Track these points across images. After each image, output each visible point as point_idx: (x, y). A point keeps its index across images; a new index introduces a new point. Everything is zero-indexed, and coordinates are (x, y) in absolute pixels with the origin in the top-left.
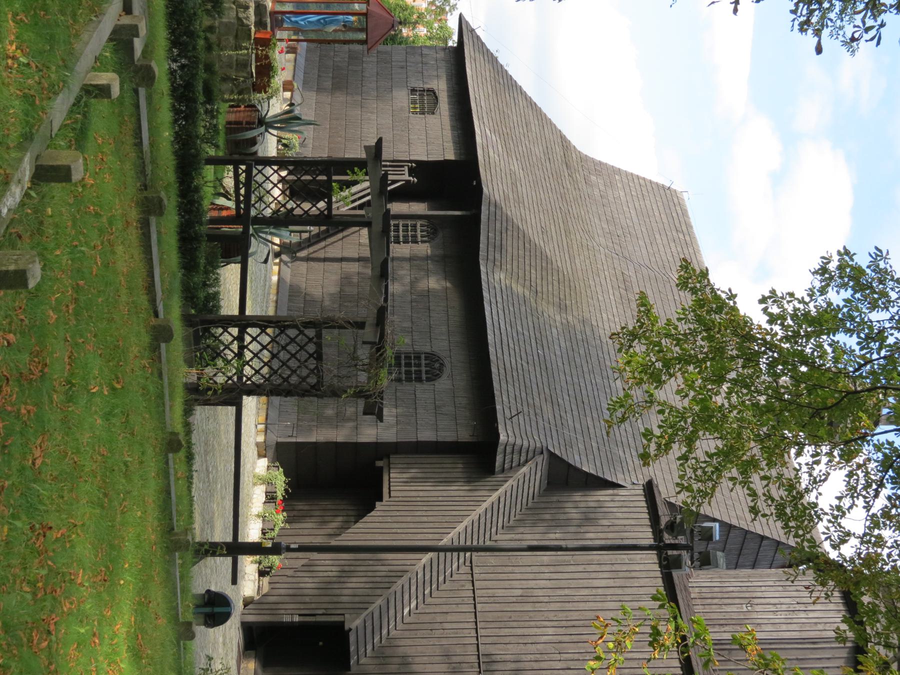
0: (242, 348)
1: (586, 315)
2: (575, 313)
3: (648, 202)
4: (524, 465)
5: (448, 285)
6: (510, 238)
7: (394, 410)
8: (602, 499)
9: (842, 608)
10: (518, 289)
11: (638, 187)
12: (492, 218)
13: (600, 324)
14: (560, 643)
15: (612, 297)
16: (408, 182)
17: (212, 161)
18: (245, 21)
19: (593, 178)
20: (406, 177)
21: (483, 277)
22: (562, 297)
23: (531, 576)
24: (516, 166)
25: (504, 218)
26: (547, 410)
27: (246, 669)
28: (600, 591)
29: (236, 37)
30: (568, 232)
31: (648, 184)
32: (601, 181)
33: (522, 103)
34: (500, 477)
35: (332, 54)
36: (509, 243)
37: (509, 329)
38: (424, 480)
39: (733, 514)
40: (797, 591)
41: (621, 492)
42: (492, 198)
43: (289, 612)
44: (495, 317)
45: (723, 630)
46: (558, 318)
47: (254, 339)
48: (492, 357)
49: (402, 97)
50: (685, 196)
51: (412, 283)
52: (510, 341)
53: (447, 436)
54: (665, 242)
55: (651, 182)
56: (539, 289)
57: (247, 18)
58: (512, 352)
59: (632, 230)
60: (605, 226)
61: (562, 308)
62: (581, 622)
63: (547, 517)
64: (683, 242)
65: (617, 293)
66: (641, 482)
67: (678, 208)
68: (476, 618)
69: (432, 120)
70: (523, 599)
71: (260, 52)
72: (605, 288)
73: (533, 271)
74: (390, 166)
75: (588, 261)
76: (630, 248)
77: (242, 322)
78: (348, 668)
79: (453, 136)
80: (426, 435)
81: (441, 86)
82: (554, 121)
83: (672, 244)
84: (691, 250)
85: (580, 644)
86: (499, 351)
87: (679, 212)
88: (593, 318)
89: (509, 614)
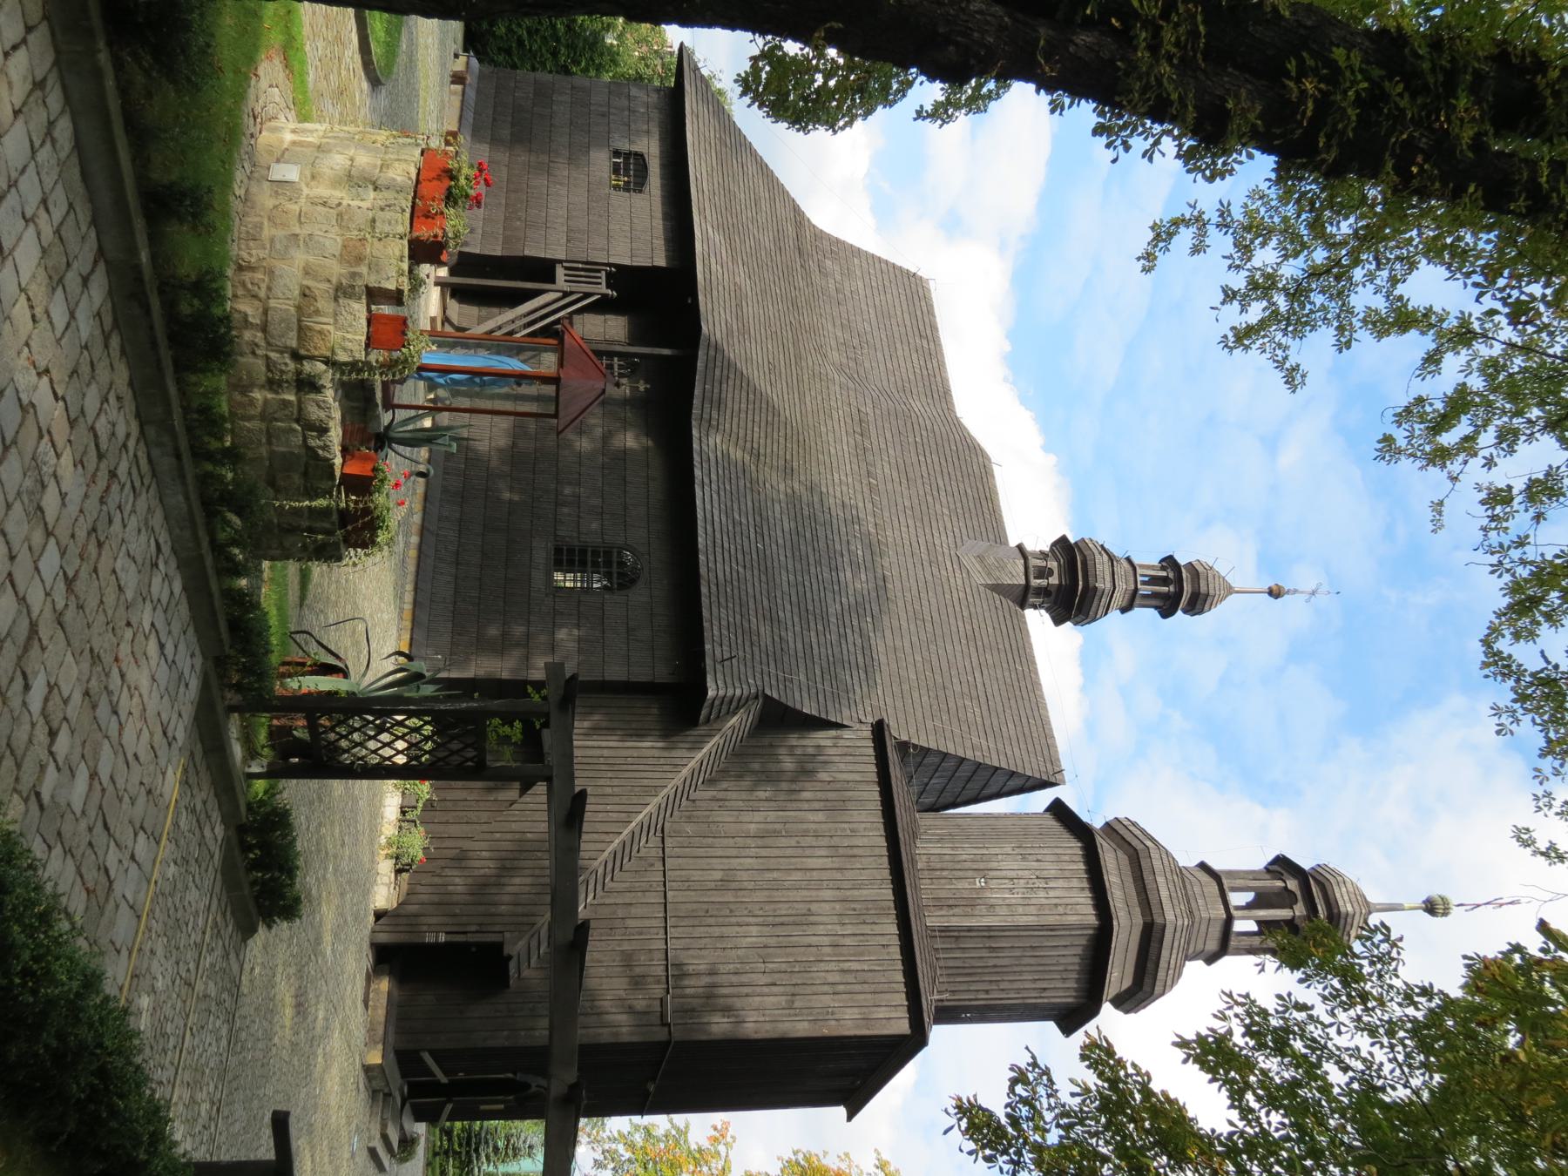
1: (816, 478)
2: (802, 478)
3: (889, 296)
4: (735, 714)
5: (650, 443)
6: (730, 389)
7: (576, 632)
8: (823, 743)
9: (1086, 885)
10: (737, 454)
11: (879, 273)
12: (711, 365)
13: (831, 491)
14: (765, 947)
15: (845, 448)
16: (604, 296)
18: (320, 452)
19: (828, 263)
20: (603, 289)
21: (696, 446)
22: (788, 457)
23: (734, 852)
24: (742, 278)
25: (726, 363)
26: (764, 630)
27: (377, 991)
29: (305, 474)
30: (798, 357)
31: (891, 270)
32: (837, 268)
33: (752, 169)
34: (701, 730)
35: (512, 85)
36: (730, 395)
37: (724, 519)
38: (610, 730)
39: (968, 744)
40: (1038, 861)
41: (846, 734)
42: (712, 339)
43: (433, 928)
44: (708, 507)
45: (951, 912)
46: (782, 487)
48: (703, 570)
49: (601, 162)
50: (932, 285)
51: (606, 437)
52: (725, 538)
53: (641, 674)
54: (907, 353)
55: (894, 266)
56: (762, 451)
57: (325, 448)
58: (726, 554)
59: (869, 337)
60: (839, 334)
61: (788, 471)
62: (791, 919)
63: (756, 766)
64: (927, 351)
65: (852, 441)
66: (870, 720)
67: (923, 303)
68: (666, 911)
69: (638, 200)
70: (725, 884)
71: (352, 505)
72: (838, 434)
73: (756, 429)
74: (582, 270)
75: (820, 398)
76: (867, 365)
78: (508, 986)
79: (665, 229)
80: (615, 672)
81: (651, 147)
82: (787, 187)
83: (915, 356)
84: (935, 365)
85: (788, 950)
86: (711, 558)
87: (924, 309)
88: (823, 482)
89: (705, 906)
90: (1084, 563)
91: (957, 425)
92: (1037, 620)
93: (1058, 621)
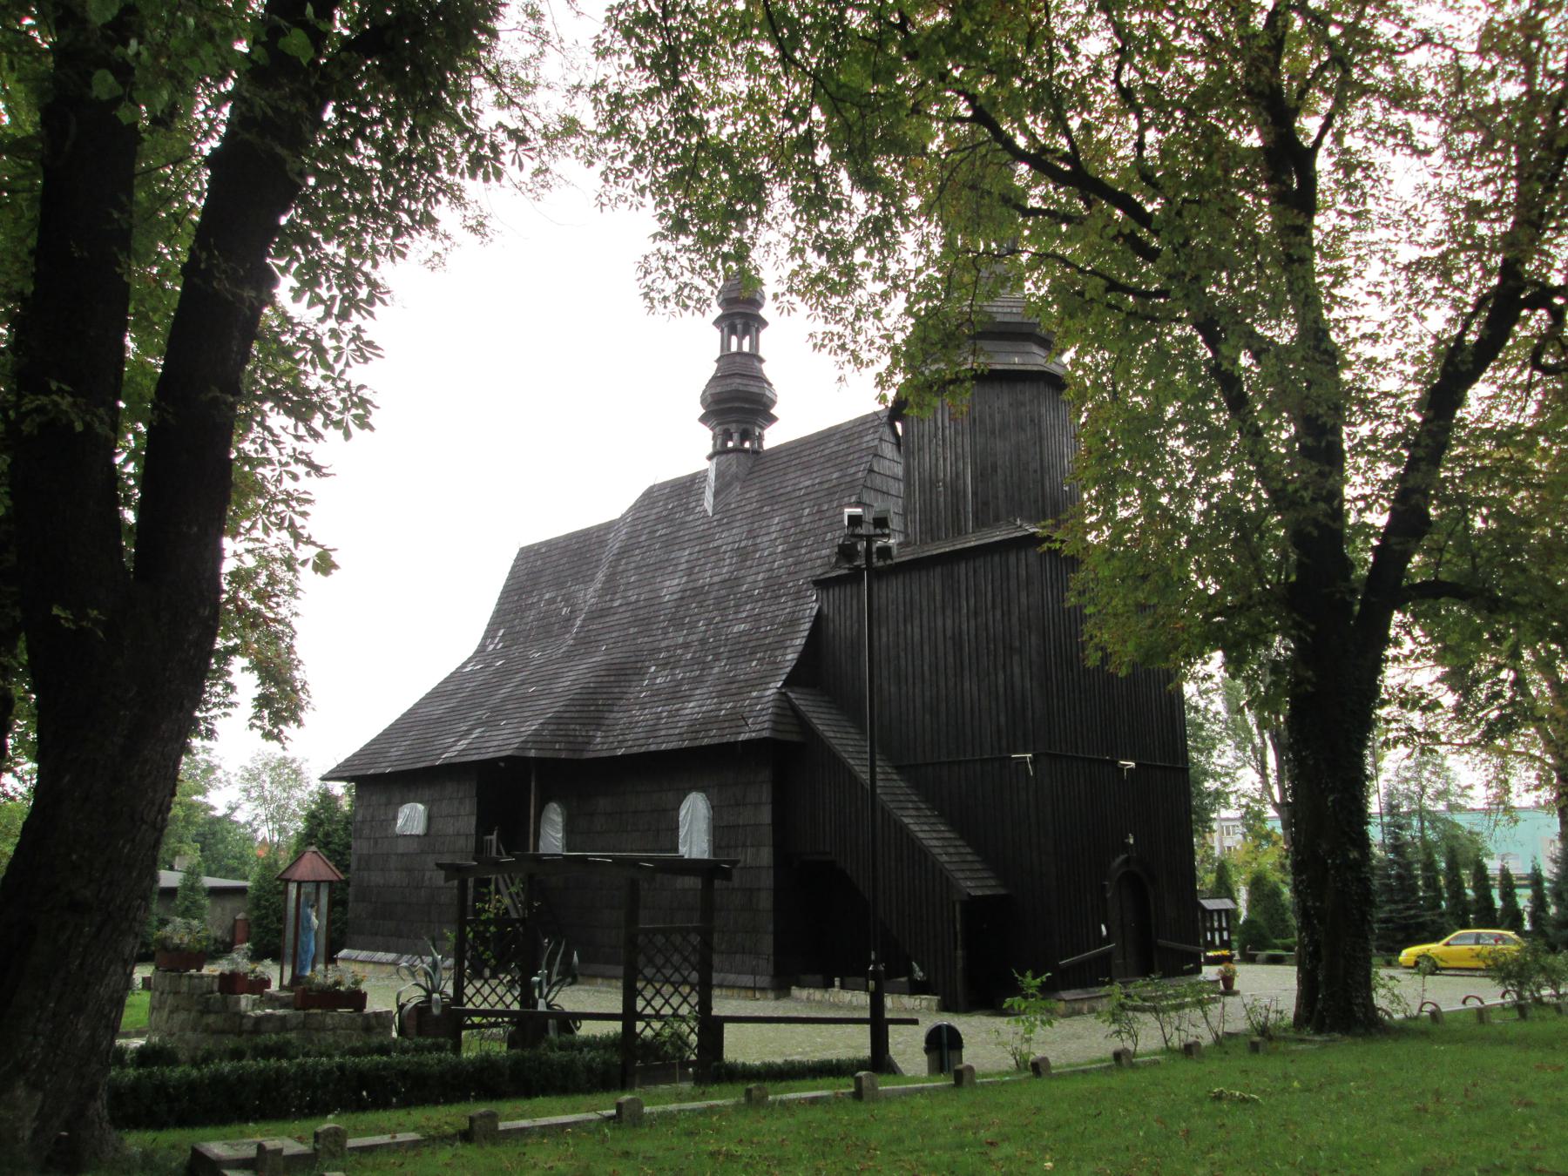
0: (658, 1016)
17: (1268, 512)
20: (494, 837)
28: (926, 633)
47: (649, 1003)
53: (766, 794)
77: (629, 1015)
90: (733, 399)
91: (623, 517)
92: (773, 437)
93: (773, 419)
